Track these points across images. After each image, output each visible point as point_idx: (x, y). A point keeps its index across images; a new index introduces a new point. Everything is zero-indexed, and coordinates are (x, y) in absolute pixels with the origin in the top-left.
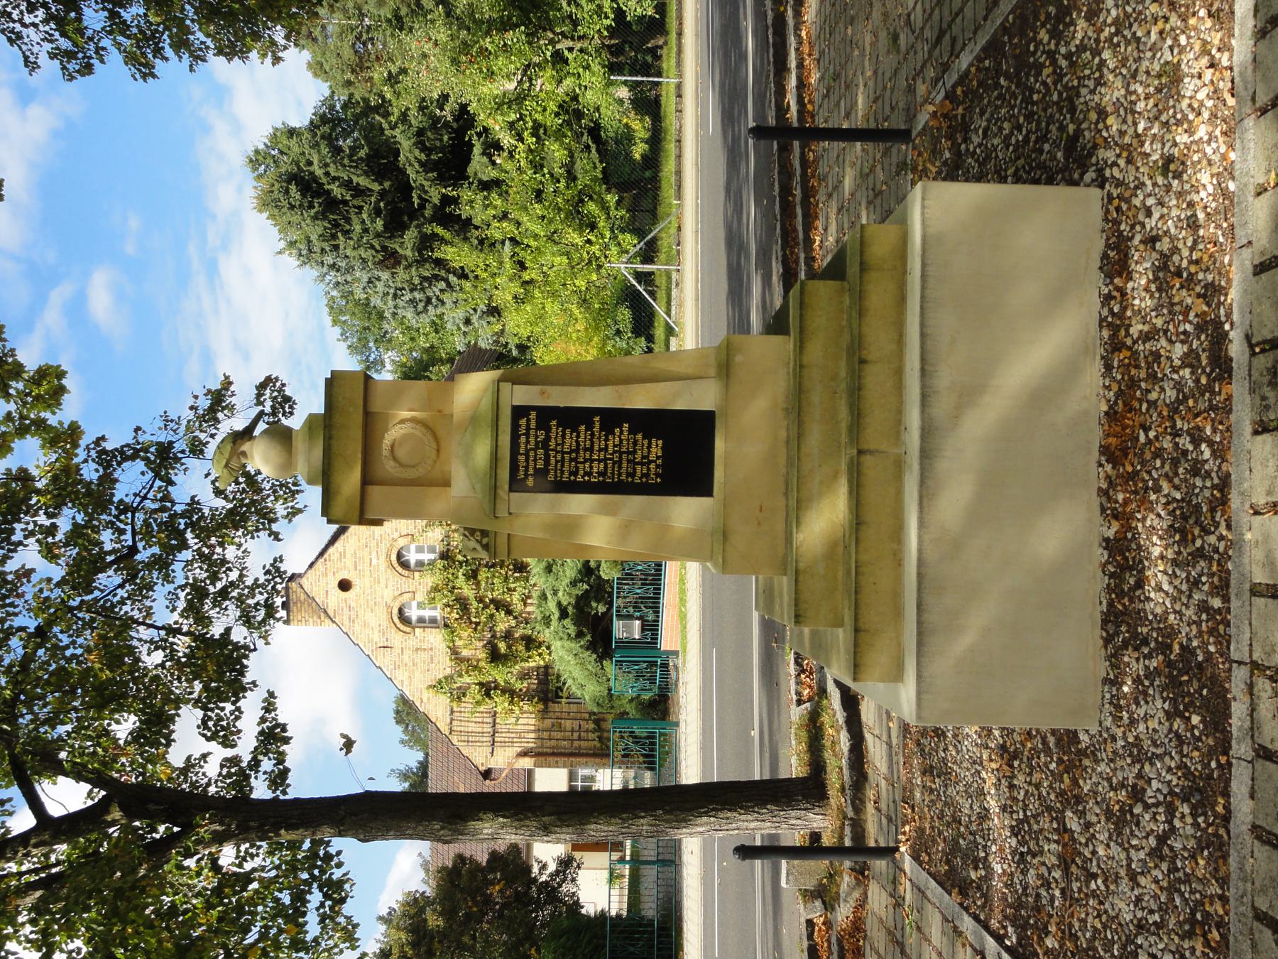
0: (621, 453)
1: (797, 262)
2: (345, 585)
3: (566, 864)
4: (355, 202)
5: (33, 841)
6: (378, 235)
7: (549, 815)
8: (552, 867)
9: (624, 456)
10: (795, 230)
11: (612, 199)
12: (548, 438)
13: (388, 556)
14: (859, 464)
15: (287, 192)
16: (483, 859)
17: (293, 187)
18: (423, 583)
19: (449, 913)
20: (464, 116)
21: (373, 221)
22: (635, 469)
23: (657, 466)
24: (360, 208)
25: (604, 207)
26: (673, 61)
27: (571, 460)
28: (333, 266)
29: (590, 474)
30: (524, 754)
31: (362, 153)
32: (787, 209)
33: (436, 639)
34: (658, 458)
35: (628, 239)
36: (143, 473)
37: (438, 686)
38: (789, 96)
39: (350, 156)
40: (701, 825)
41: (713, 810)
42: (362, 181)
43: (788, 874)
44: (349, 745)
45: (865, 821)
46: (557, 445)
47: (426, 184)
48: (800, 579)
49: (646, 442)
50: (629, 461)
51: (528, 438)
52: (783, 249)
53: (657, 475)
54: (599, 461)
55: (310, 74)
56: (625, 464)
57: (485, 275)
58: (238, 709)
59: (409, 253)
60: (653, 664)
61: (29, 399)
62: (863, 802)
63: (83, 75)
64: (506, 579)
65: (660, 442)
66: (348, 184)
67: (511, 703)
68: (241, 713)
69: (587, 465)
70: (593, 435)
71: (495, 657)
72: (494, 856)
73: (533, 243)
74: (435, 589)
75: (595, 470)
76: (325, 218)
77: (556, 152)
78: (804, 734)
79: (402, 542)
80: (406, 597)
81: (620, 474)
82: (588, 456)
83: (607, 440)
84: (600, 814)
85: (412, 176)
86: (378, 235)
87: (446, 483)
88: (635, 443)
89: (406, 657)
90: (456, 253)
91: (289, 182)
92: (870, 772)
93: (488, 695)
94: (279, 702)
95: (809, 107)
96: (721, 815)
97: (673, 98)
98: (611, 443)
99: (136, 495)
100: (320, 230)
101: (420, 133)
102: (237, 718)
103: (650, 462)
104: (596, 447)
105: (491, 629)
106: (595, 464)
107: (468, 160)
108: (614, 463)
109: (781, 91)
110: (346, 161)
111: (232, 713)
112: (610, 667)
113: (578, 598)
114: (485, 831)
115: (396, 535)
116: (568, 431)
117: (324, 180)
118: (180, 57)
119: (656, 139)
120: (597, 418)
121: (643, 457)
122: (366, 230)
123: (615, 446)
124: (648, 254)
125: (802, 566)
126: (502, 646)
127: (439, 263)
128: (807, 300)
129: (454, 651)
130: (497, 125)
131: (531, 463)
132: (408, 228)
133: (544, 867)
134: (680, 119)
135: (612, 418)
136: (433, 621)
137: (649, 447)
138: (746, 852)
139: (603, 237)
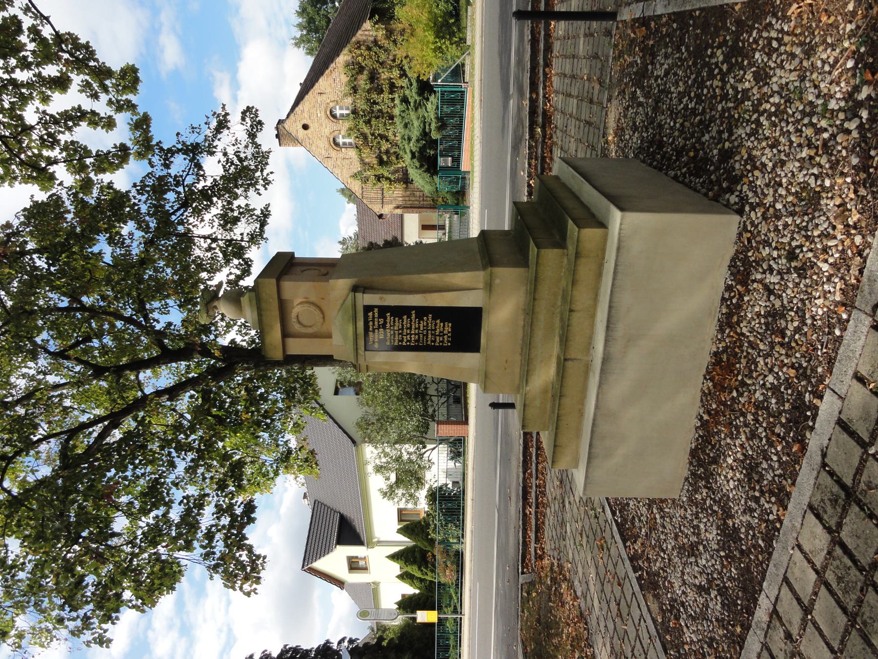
1: (539, 33)
2: (305, 127)
12: (385, 323)
13: (326, 112)
14: (564, 366)
18: (346, 125)
27: (399, 334)
29: (410, 341)
30: (398, 207)
33: (352, 153)
36: (185, 159)
37: (354, 176)
53: (448, 341)
54: (415, 334)
56: (430, 336)
60: (458, 179)
61: (120, 88)
64: (385, 124)
67: (390, 184)
71: (381, 163)
74: (350, 129)
79: (332, 105)
80: (337, 132)
83: (419, 323)
87: (330, 336)
88: (436, 325)
89: (338, 162)
93: (379, 181)
98: (421, 325)
99: (183, 171)
103: (444, 335)
105: (379, 149)
106: (413, 336)
112: (437, 179)
113: (420, 148)
115: (328, 101)
126: (385, 158)
129: (362, 160)
135: (422, 312)
136: (350, 144)
137: (444, 327)
138: (495, 406)
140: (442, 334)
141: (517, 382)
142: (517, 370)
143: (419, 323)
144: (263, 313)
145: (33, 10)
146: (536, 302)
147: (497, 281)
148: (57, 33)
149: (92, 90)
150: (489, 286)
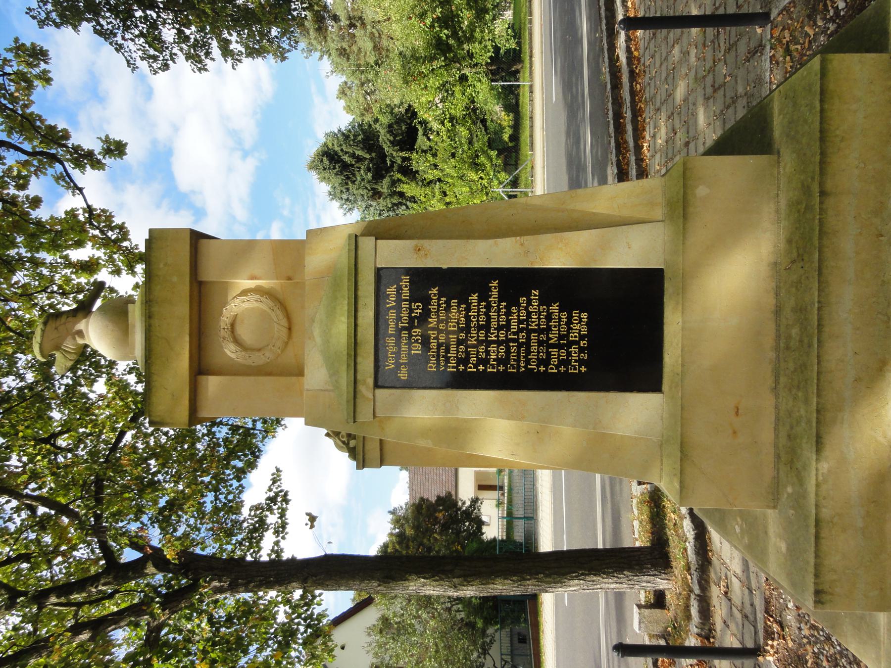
0: (529, 332)
1: (628, 164)
3: (475, 501)
4: (357, 165)
5: (102, 581)
6: (369, 182)
8: (468, 503)
9: (533, 336)
10: (626, 142)
11: (494, 153)
12: (426, 314)
15: (322, 161)
16: (433, 499)
17: (325, 158)
19: (416, 528)
20: (411, 113)
21: (366, 174)
22: (549, 354)
23: (582, 350)
24: (360, 168)
25: (490, 159)
26: (527, 46)
27: (459, 343)
28: (347, 200)
29: (485, 362)
31: (360, 138)
32: (619, 129)
34: (582, 337)
35: (503, 176)
38: (618, 51)
39: (353, 140)
40: (573, 586)
41: (582, 574)
42: (359, 153)
43: (640, 623)
44: (312, 519)
45: (710, 598)
46: (439, 322)
47: (394, 153)
48: (824, 533)
49: (564, 315)
50: (540, 343)
51: (399, 312)
52: (617, 156)
53: (581, 362)
54: (499, 343)
55: (345, 112)
56: (534, 348)
57: (425, 200)
58: (241, 486)
59: (385, 190)
62: (708, 582)
65: (584, 316)
66: (353, 155)
68: (243, 488)
69: (482, 349)
70: (488, 307)
72: (439, 498)
73: (450, 180)
75: (493, 356)
76: (342, 174)
77: (463, 132)
78: (646, 509)
81: (528, 362)
83: (508, 313)
84: (496, 577)
85: (386, 149)
86: (369, 182)
87: (299, 372)
88: (549, 318)
90: (409, 189)
91: (323, 156)
92: (714, 560)
94: (283, 475)
95: (636, 54)
96: (588, 578)
97: (527, 94)
100: (340, 181)
101: (390, 126)
102: (241, 492)
103: (571, 344)
104: (494, 324)
106: (493, 348)
107: (415, 140)
108: (520, 346)
109: (612, 48)
110: (351, 143)
114: (411, 588)
116: (454, 302)
117: (341, 154)
118: (226, 61)
119: (517, 126)
120: (495, 284)
121: (561, 337)
122: (363, 180)
123: (520, 322)
124: (515, 183)
125: (825, 513)
127: (402, 195)
128: (831, 86)
130: (428, 116)
131: (404, 347)
132: (384, 177)
133: (464, 503)
134: (532, 105)
135: (516, 282)
137: (569, 322)
139: (488, 174)
140: (565, 343)
141: (768, 472)
142: (767, 435)
144: (155, 309)
145: (67, 179)
146: (830, 202)
147: (701, 191)
148: (89, 206)
149: (114, 265)
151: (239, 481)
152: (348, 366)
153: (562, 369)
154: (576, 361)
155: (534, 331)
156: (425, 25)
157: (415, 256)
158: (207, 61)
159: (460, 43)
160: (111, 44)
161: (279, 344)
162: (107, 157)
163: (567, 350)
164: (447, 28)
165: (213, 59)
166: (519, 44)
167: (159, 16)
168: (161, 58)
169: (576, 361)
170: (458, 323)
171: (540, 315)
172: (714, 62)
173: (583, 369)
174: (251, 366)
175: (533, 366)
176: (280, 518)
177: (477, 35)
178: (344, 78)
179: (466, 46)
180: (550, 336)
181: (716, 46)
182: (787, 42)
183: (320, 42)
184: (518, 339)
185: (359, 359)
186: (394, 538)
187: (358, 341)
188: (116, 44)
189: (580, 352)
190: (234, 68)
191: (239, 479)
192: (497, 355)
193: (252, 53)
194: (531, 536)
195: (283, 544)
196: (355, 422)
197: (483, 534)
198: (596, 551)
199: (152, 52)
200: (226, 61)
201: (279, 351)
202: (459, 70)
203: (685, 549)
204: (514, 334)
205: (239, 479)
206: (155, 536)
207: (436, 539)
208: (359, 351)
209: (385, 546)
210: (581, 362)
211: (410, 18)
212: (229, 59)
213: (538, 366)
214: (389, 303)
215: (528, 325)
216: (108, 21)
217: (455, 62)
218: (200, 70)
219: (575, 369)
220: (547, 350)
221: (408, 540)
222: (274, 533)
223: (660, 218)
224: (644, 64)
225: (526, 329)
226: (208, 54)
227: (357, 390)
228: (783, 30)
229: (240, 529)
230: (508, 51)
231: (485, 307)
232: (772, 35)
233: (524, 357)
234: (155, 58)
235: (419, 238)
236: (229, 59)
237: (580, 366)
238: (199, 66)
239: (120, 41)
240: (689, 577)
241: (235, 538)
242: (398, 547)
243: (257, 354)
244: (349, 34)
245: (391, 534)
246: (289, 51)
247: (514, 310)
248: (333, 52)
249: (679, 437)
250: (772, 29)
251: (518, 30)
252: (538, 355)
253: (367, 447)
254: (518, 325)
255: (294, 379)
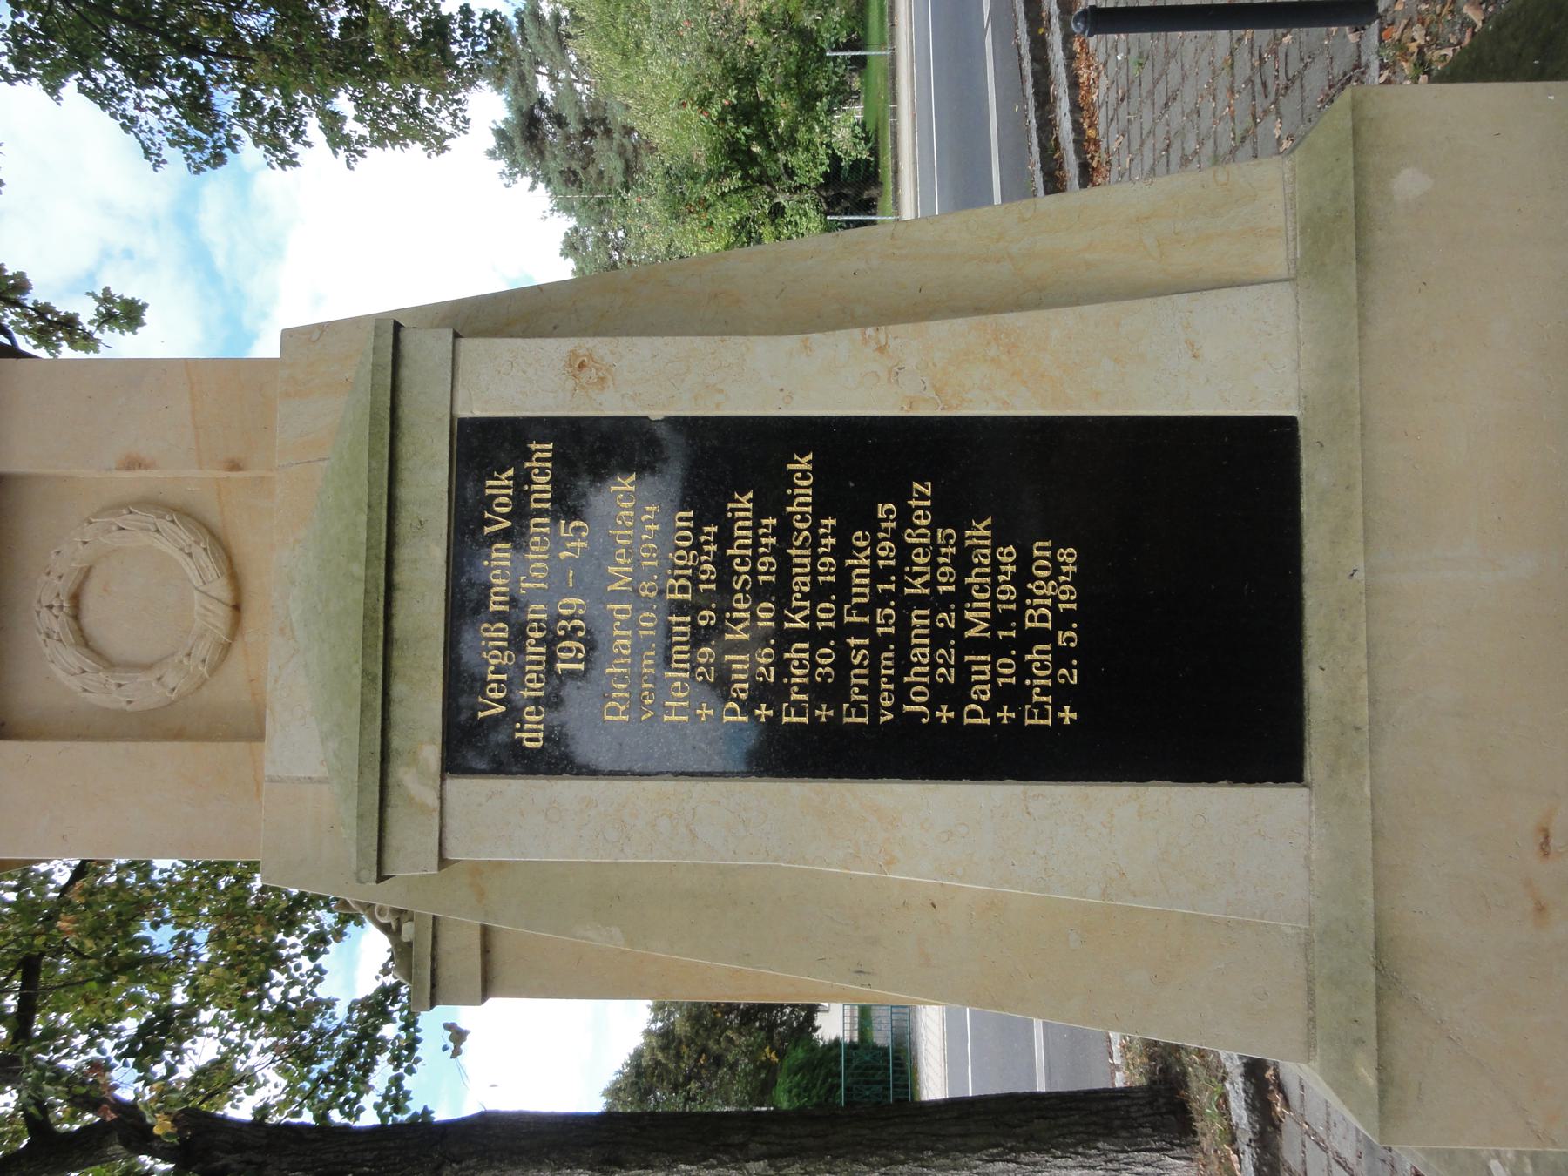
0: (906, 604)
7: (758, 1159)
22: (964, 670)
23: (1061, 657)
34: (1062, 620)
41: (1012, 1150)
49: (1008, 555)
50: (939, 638)
54: (816, 638)
56: (920, 653)
58: (318, 968)
63: (214, 167)
65: (1068, 556)
68: (323, 972)
69: (765, 657)
70: (785, 531)
75: (799, 676)
82: (766, 621)
83: (843, 550)
88: (963, 562)
95: (1091, 133)
102: (317, 981)
103: (1029, 639)
104: (801, 581)
106: (798, 652)
109: (1047, 125)
111: (310, 974)
120: (805, 463)
121: (999, 620)
123: (878, 575)
135: (866, 461)
137: (1022, 577)
143: (843, 550)
147: (1408, 183)
150: (1346, 240)
151: (312, 959)
152: (365, 706)
153: (1005, 715)
154: (1045, 691)
155: (920, 601)
156: (709, 117)
157: (570, 384)
158: (296, 148)
159: (772, 150)
160: (113, 115)
161: (204, 649)
162: (106, 327)
163: (1019, 659)
164: (747, 125)
165: (308, 144)
166: (874, 152)
167: (208, 70)
168: (210, 144)
169: (1045, 691)
170: (695, 580)
171: (936, 553)
172: (1254, 118)
173: (1067, 715)
174: (121, 713)
175: (918, 705)
176: (405, 1028)
177: (802, 135)
178: (573, 222)
179: (782, 157)
180: (969, 615)
181: (1258, 87)
182: (1420, 48)
183: (533, 160)
184: (873, 624)
185: (399, 689)
186: (654, 1040)
187: (397, 634)
188: (124, 116)
189: (1057, 665)
190: (349, 167)
191: (313, 954)
192: (811, 675)
193: (383, 138)
194: (904, 1035)
195: (408, 1083)
196: (381, 878)
197: (815, 1029)
198: (1035, 1097)
199: (193, 132)
200: (335, 153)
201: (204, 670)
202: (770, 196)
203: (1224, 1096)
204: (861, 609)
205: (313, 954)
206: (126, 1084)
207: (730, 1040)
208: (397, 663)
209: (638, 1055)
210: (1061, 694)
211: (684, 104)
212: (342, 153)
213: (933, 705)
214: (490, 522)
215: (901, 584)
216: (111, 71)
217: (762, 183)
218: (283, 164)
219: (1043, 715)
220: (959, 658)
221: (680, 1042)
222: (391, 1061)
223: (1282, 272)
224: (1107, 150)
225: (897, 595)
226: (297, 135)
227: (391, 781)
228: (1409, 25)
229: (330, 1047)
230: (856, 164)
231: (775, 531)
232: (1381, 40)
233: (890, 679)
234: (199, 144)
235: (582, 333)
236: (342, 153)
237: (1057, 707)
238: (282, 156)
239: (131, 110)
240: (1234, 1157)
241: (316, 1067)
242: (660, 1056)
243: (141, 678)
244: (583, 147)
245: (648, 1033)
246: (452, 136)
247: (859, 539)
248: (555, 176)
249: (1370, 921)
250: (1381, 30)
251: (870, 135)
252: (932, 674)
253: (445, 945)
254: (873, 586)
255: (240, 747)
